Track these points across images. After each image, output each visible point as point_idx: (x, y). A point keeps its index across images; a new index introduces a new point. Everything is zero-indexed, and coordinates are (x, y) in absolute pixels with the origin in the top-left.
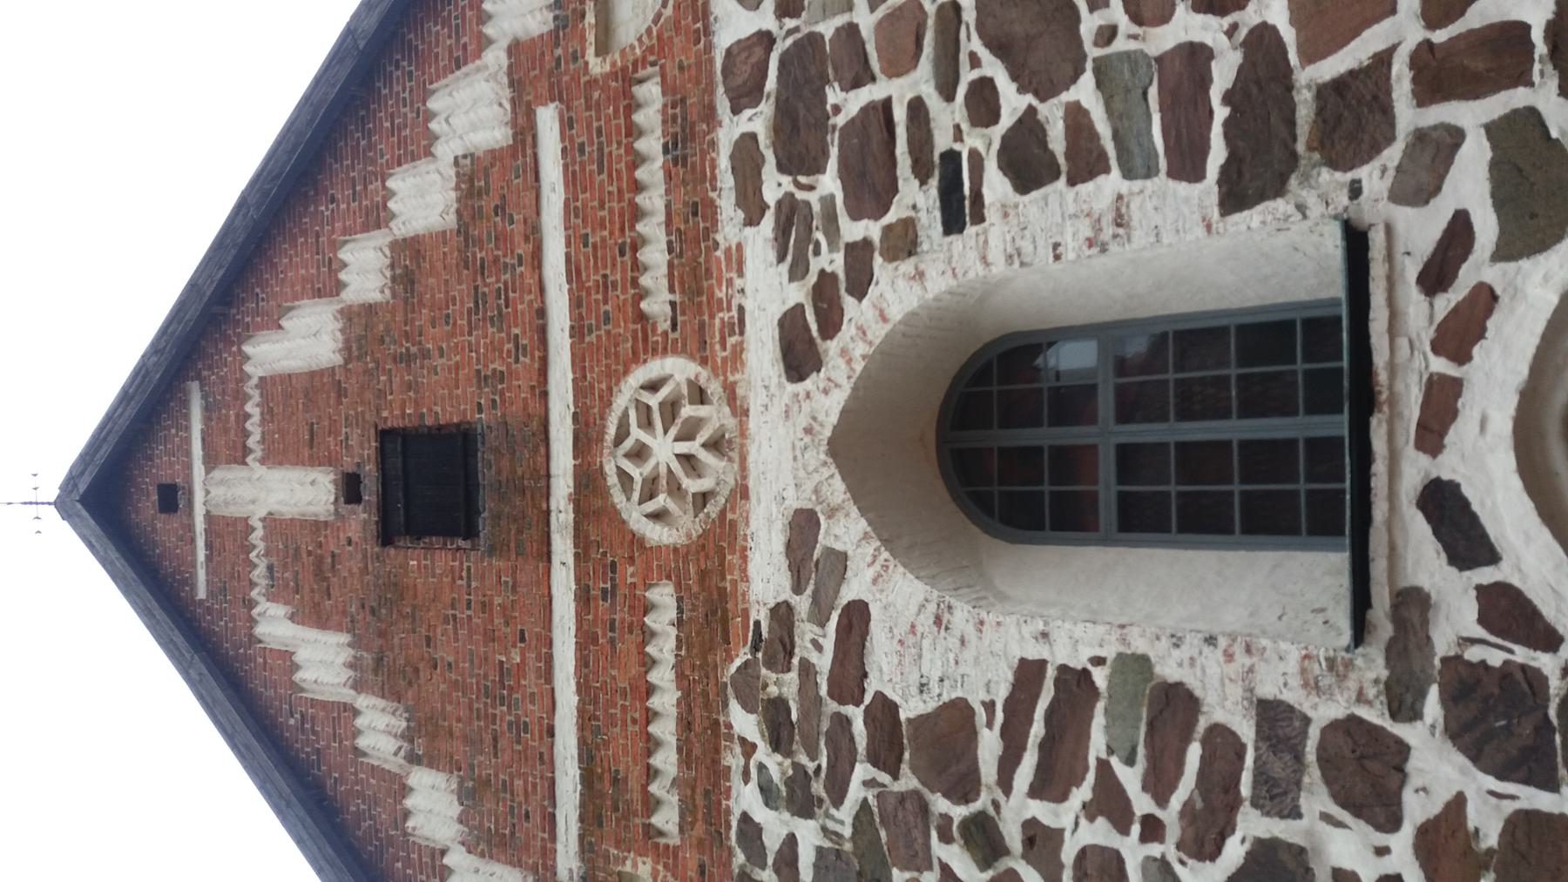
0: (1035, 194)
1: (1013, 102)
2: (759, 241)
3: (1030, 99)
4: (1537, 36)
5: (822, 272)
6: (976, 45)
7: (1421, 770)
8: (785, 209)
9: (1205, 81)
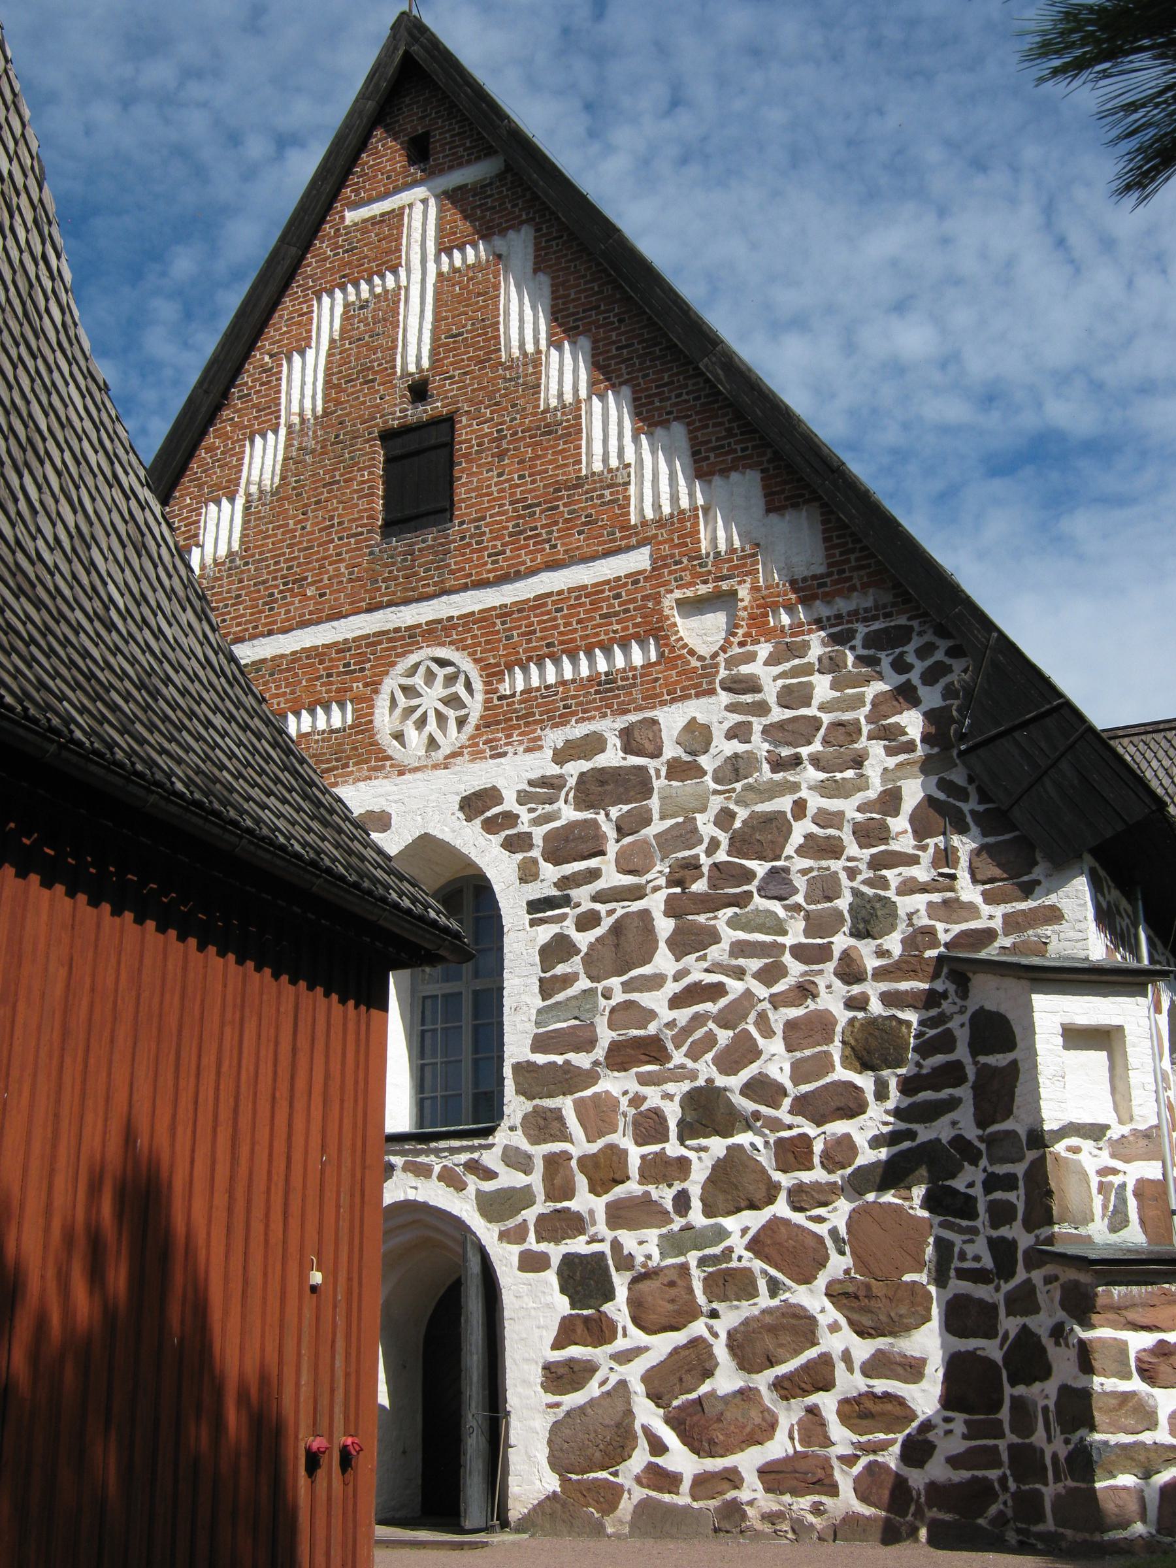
0: (537, 958)
1: (583, 940)
2: (542, 764)
3: (584, 949)
4: (566, 1204)
5: (518, 816)
6: (620, 912)
7: (129, 1135)
8: (555, 781)
9: (577, 1049)
